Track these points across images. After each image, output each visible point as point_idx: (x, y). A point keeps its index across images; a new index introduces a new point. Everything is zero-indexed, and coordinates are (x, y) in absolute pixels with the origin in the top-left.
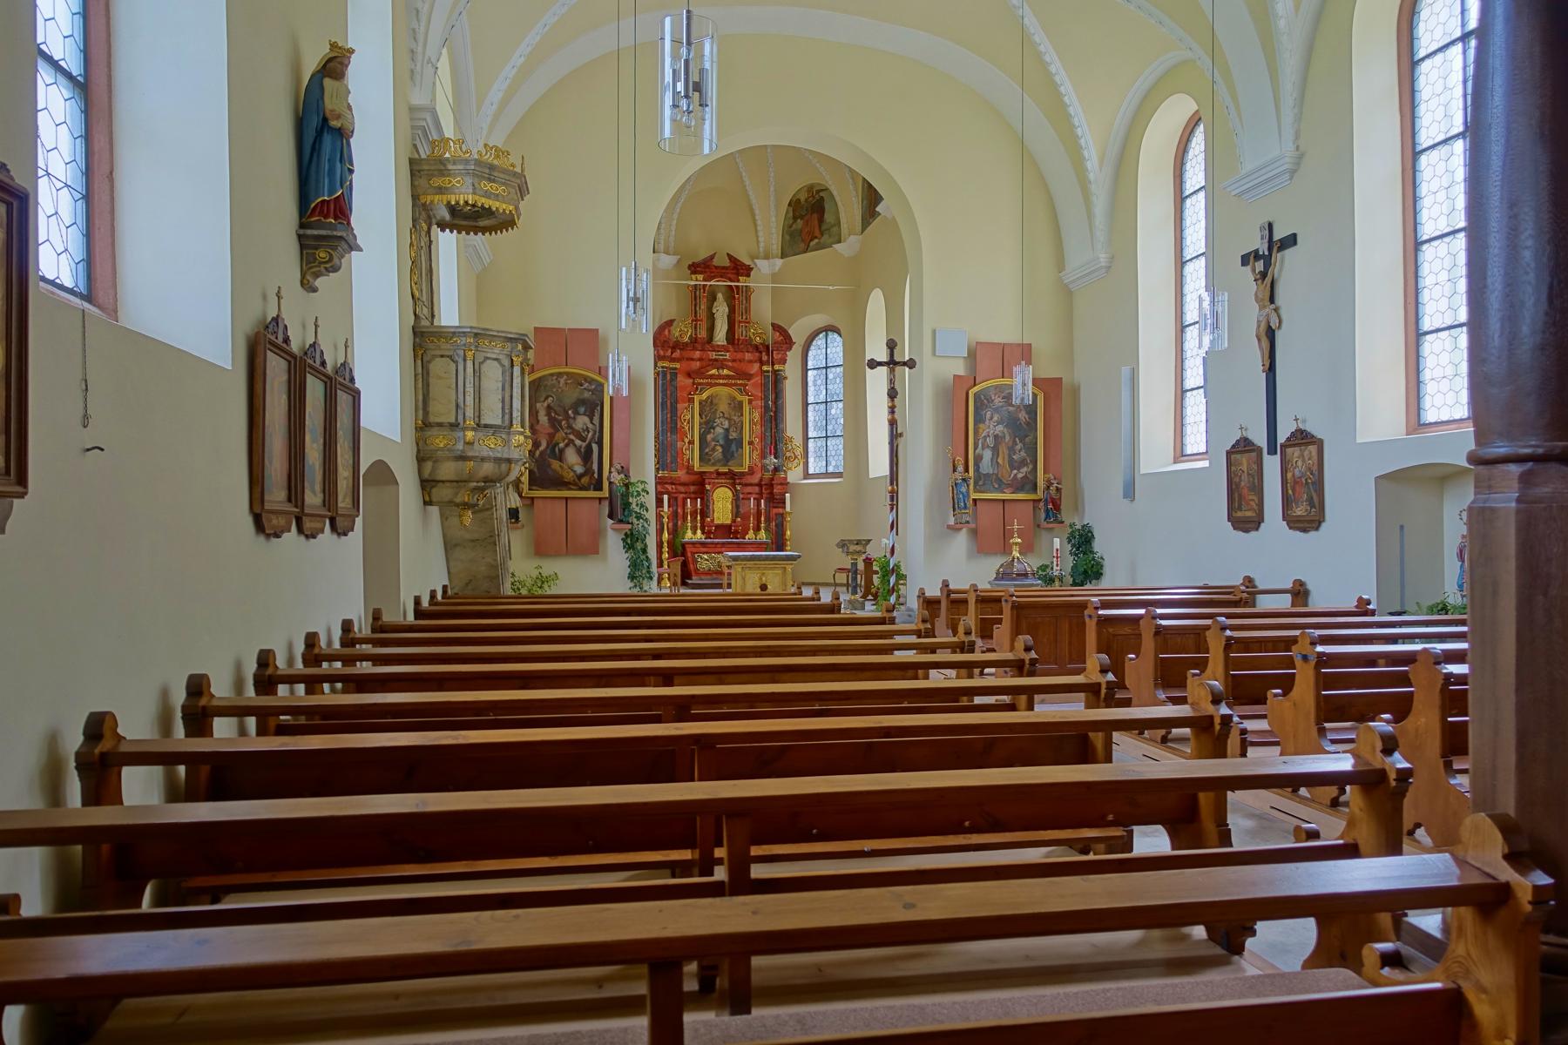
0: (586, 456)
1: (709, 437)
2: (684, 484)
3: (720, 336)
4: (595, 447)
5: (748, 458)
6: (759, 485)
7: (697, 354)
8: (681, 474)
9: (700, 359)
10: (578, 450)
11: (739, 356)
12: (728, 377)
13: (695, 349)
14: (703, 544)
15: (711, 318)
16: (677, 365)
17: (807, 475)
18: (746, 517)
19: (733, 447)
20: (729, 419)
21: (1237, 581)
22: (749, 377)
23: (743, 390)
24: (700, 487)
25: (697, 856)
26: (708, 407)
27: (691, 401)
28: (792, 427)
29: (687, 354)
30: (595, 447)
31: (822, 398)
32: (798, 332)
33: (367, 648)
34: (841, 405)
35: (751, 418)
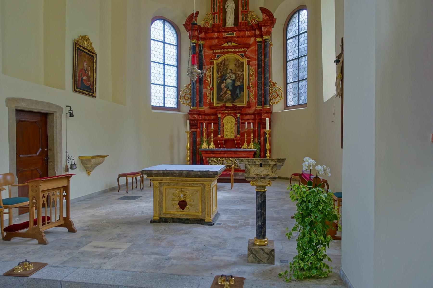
0: (237, 117)
1: (223, 85)
2: (206, 115)
3: (230, 23)
5: (247, 97)
6: (254, 114)
7: (216, 35)
8: (206, 109)
9: (217, 38)
11: (242, 33)
12: (234, 47)
13: (213, 32)
14: (212, 152)
15: (224, 11)
17: (286, 107)
18: (242, 135)
19: (238, 91)
20: (235, 74)
22: (248, 46)
23: (244, 55)
24: (215, 117)
26: (222, 66)
27: (212, 63)
28: (276, 76)
29: (209, 35)
31: (296, 56)
33: (134, 180)
35: (249, 74)
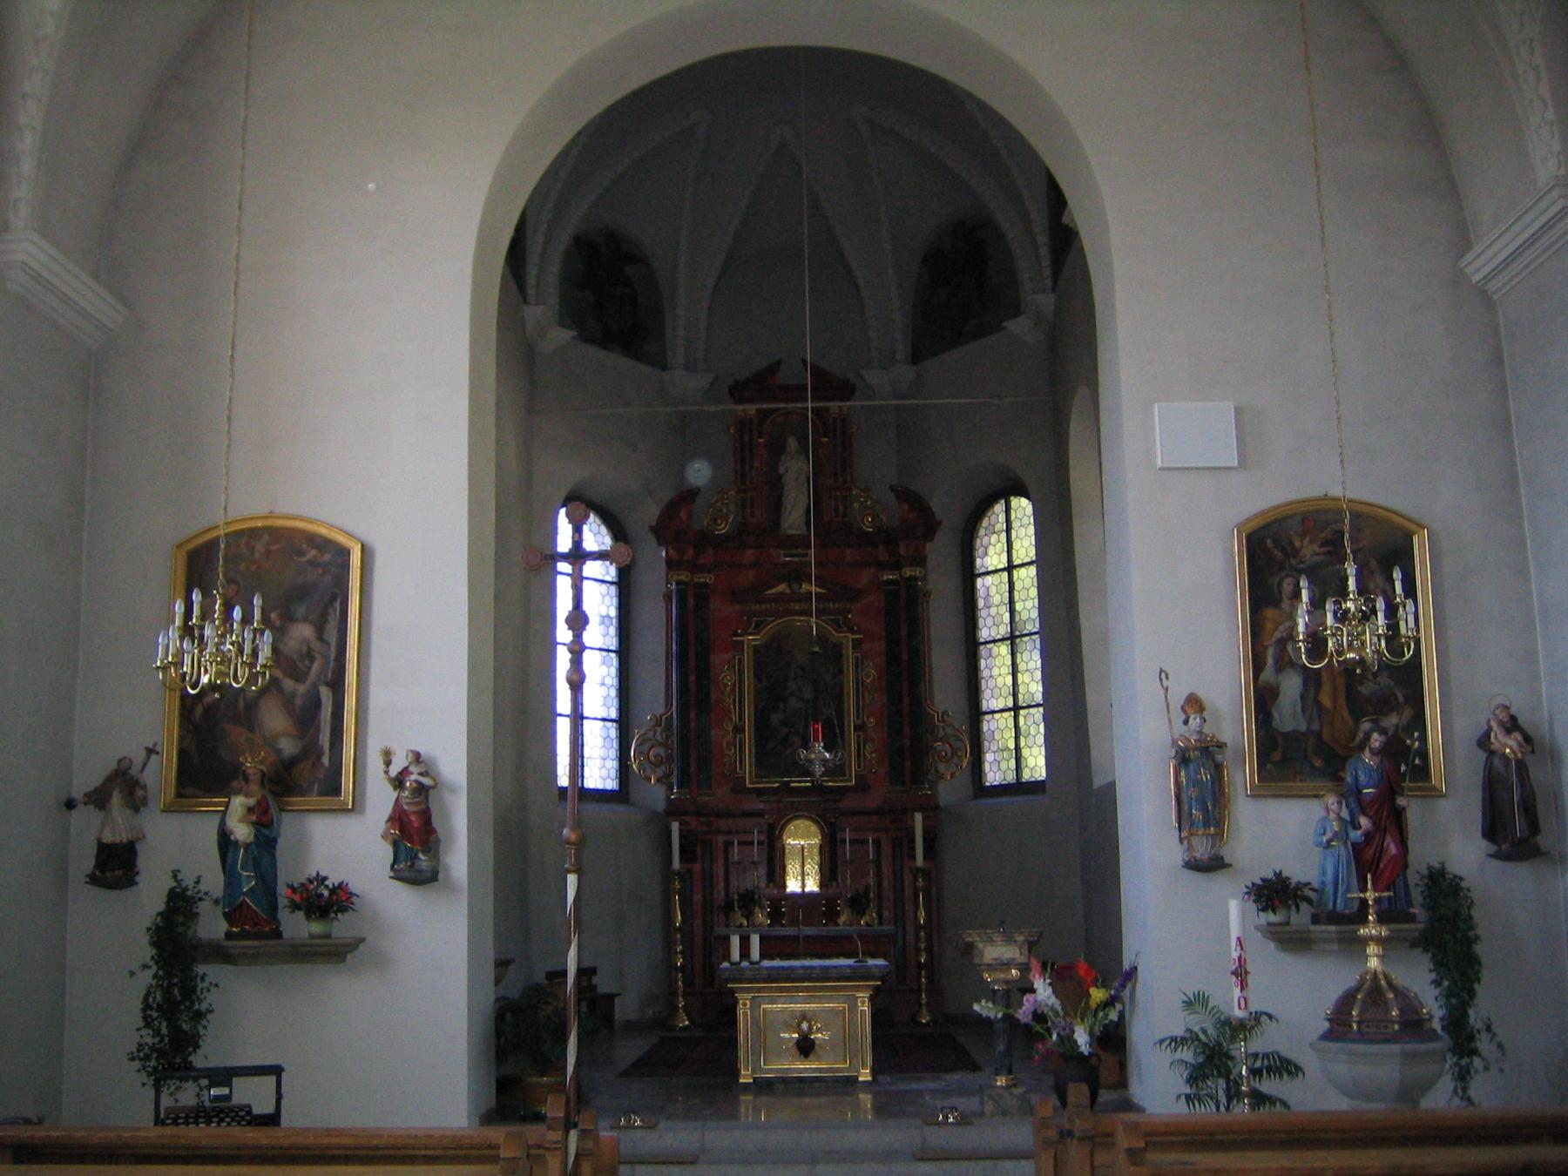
1: (775, 718)
3: (795, 514)
4: (326, 694)
10: (288, 703)
16: (707, 578)
21: (114, 766)
25: (1000, 1015)
30: (326, 694)
32: (945, 503)
34: (1033, 570)
